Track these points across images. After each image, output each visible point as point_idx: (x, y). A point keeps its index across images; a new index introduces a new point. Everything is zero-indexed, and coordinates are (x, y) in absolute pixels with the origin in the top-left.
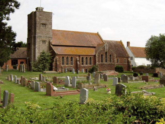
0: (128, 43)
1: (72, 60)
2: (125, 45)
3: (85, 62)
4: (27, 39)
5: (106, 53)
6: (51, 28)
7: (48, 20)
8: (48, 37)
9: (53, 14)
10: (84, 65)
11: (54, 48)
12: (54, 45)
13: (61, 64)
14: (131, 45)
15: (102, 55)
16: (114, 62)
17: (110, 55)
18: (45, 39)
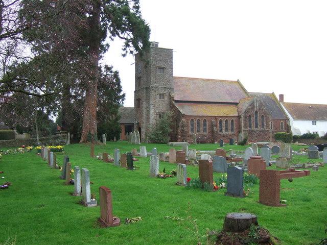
0: (281, 96)
1: (205, 125)
2: (278, 98)
3: (224, 128)
4: (135, 92)
5: (256, 112)
6: (172, 74)
7: (166, 61)
8: (168, 88)
9: (174, 52)
10: (253, 129)
11: (178, 106)
12: (177, 101)
13: (190, 132)
14: (286, 100)
15: (250, 116)
16: (268, 127)
17: (263, 116)
18: (162, 92)
